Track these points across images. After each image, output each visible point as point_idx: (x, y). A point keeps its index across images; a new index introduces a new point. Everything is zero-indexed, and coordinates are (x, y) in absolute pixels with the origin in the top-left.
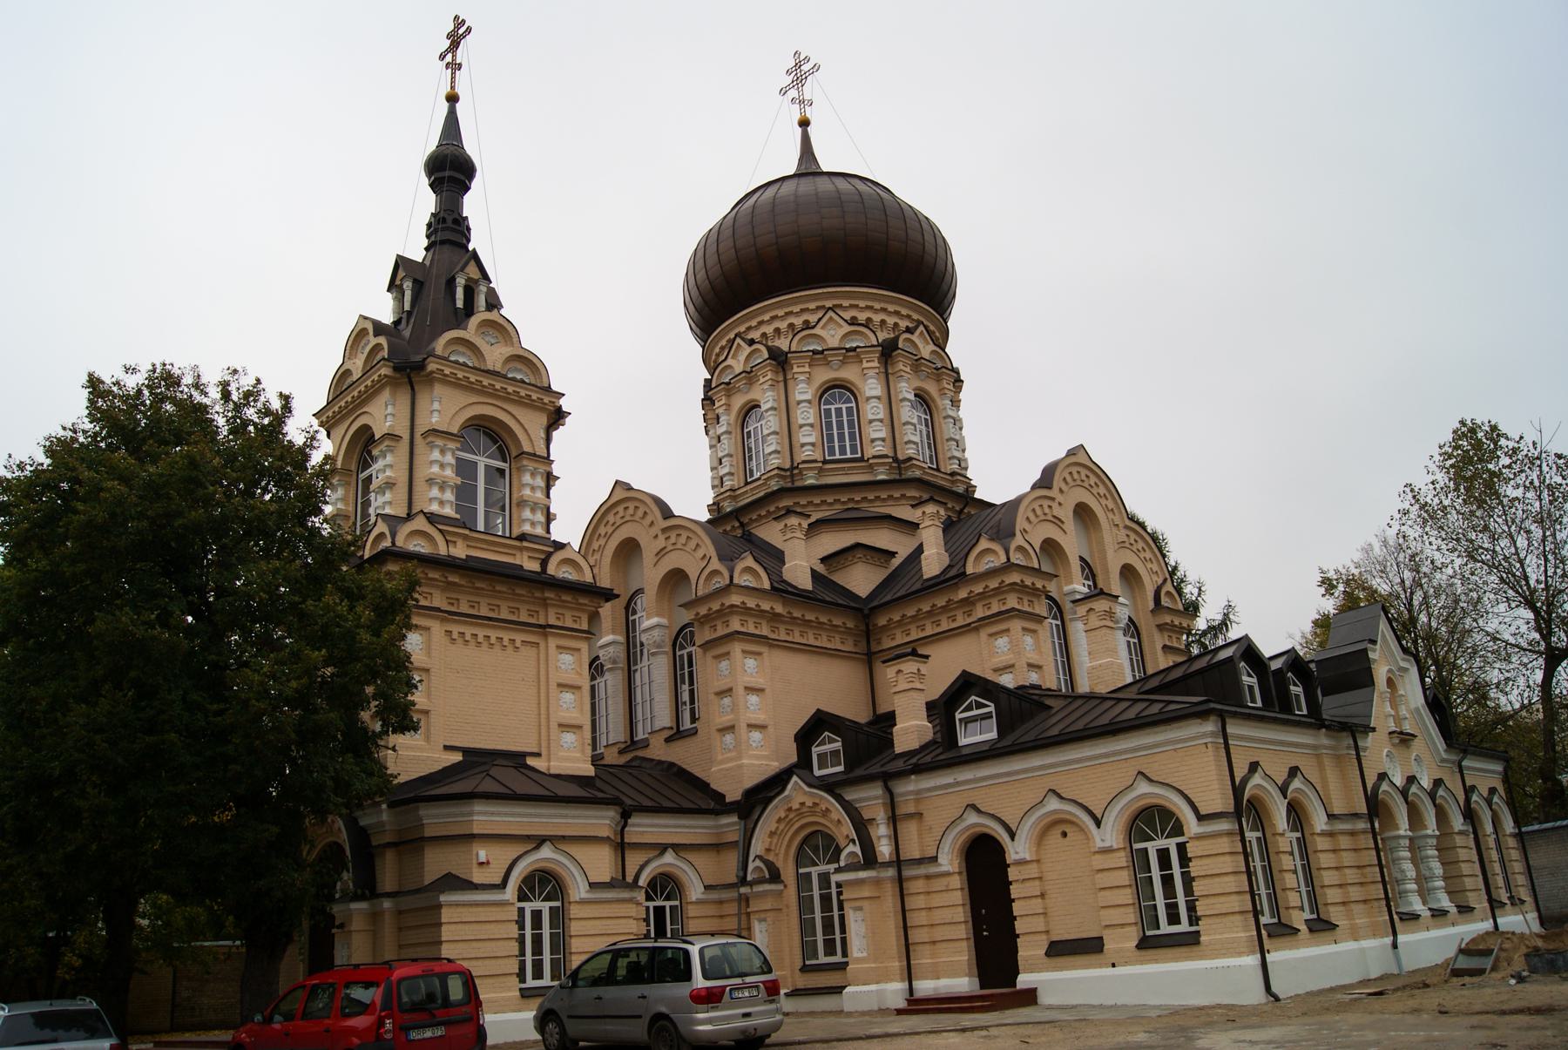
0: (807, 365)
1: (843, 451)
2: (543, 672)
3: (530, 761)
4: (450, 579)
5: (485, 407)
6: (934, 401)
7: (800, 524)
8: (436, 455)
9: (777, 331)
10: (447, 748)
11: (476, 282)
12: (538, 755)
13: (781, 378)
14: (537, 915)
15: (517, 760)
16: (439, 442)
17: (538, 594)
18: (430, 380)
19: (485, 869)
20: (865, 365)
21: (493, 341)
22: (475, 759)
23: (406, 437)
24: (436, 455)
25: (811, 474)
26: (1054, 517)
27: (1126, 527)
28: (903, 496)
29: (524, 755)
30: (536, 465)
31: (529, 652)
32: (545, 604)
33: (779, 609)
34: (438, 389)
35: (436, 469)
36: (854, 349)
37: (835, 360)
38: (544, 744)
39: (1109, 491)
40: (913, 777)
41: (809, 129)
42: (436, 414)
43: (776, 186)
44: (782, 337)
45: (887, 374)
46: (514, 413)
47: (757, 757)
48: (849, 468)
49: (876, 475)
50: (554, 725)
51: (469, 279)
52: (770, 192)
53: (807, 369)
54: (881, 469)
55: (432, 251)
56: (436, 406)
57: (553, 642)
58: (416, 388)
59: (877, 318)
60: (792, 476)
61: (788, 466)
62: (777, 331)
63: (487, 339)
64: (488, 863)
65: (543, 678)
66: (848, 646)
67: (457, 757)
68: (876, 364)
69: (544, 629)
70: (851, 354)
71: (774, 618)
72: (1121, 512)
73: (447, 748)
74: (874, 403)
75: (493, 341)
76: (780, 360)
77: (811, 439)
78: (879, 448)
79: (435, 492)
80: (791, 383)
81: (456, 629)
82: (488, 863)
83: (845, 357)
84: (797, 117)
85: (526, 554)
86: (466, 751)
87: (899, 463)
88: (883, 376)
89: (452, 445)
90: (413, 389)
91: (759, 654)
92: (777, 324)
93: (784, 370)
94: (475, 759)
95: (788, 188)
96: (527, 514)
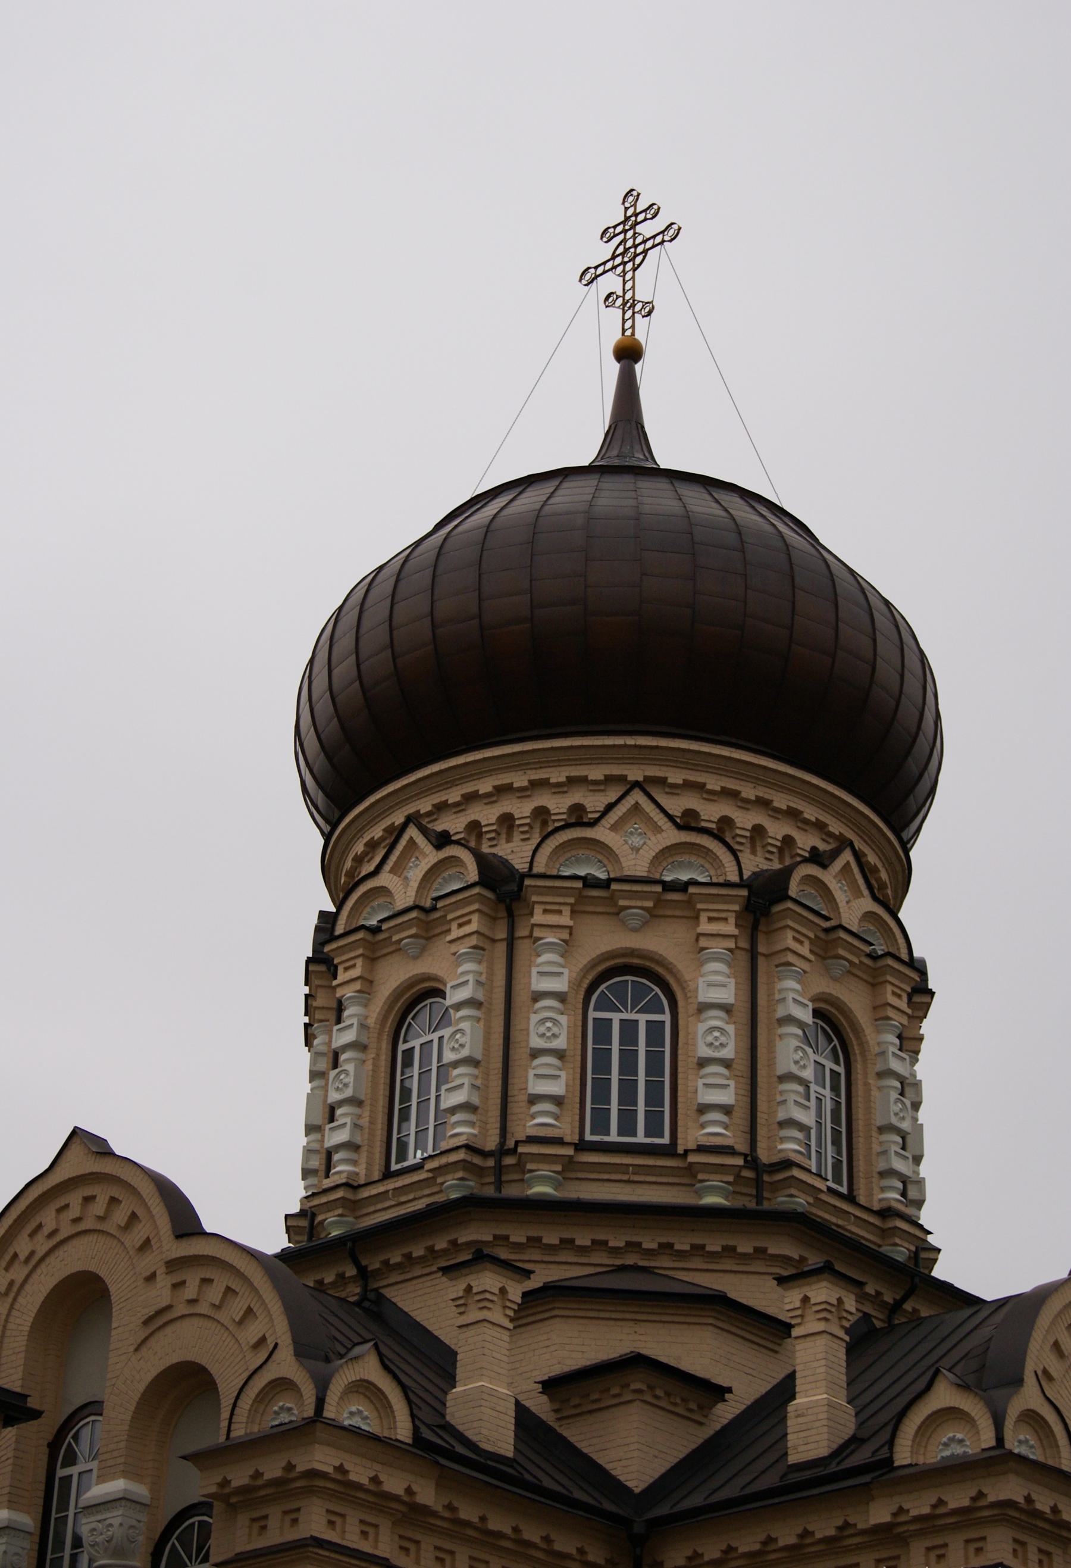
0: (566, 911)
1: (627, 1125)
9: (507, 821)
13: (502, 934)
20: (705, 927)
25: (545, 1170)
28: (760, 1252)
37: (636, 907)
41: (638, 367)
43: (549, 487)
44: (517, 837)
48: (639, 1169)
49: (699, 1194)
52: (531, 499)
54: (715, 1180)
60: (499, 1170)
68: (730, 928)
74: (715, 1019)
77: (556, 1088)
83: (659, 902)
84: (613, 336)
88: (743, 959)
92: (509, 805)
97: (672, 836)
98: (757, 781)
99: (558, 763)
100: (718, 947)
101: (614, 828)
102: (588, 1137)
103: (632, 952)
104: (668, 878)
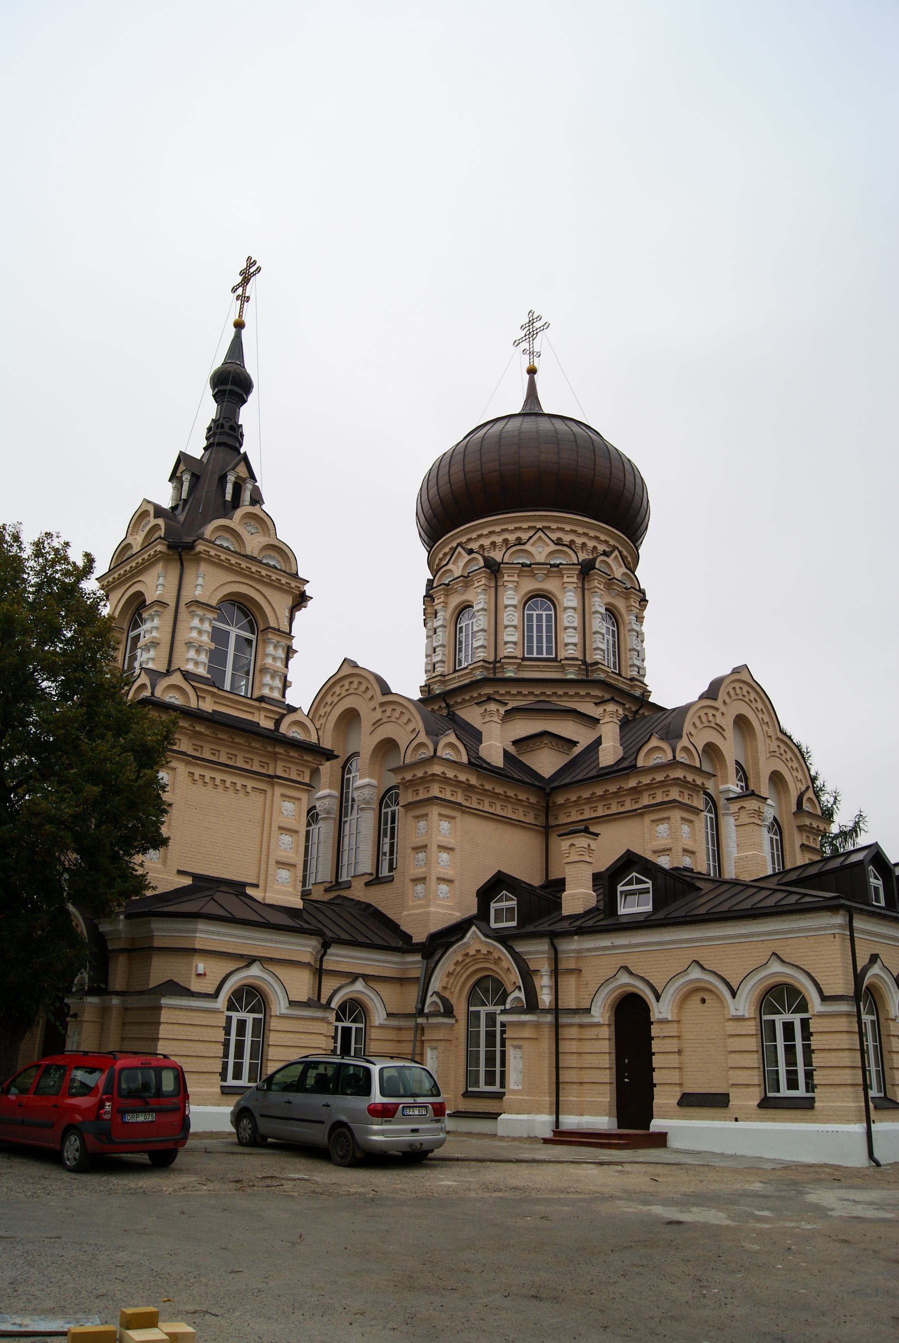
1: (540, 651)
2: (267, 816)
3: (249, 891)
4: (197, 729)
5: (245, 587)
6: (621, 615)
7: (498, 710)
8: (196, 622)
9: (493, 544)
10: (180, 872)
11: (244, 480)
12: (256, 886)
14: (242, 1024)
15: (238, 888)
16: (200, 612)
17: (270, 749)
18: (198, 559)
19: (201, 980)
21: (253, 531)
22: (203, 884)
23: (172, 605)
24: (196, 622)
25: (511, 668)
26: (717, 724)
27: (778, 739)
28: (588, 694)
29: (244, 885)
30: (279, 639)
31: (257, 798)
32: (275, 757)
33: (474, 781)
34: (204, 567)
35: (194, 634)
36: (557, 566)
37: (541, 573)
38: (262, 878)
39: (766, 706)
40: (576, 937)
42: (199, 588)
43: (505, 422)
44: (497, 550)
45: (496, 587)
46: (265, 593)
47: (443, 907)
50: (272, 862)
51: (238, 477)
52: (499, 426)
53: (515, 579)
54: (571, 670)
55: (209, 451)
56: (200, 581)
57: (278, 791)
58: (185, 565)
59: (579, 541)
60: (495, 668)
61: (491, 659)
62: (493, 544)
63: (248, 528)
64: (205, 974)
65: (267, 821)
66: (530, 819)
67: (188, 881)
68: (575, 580)
69: (272, 779)
70: (555, 569)
71: (468, 788)
72: (774, 726)
73: (180, 872)
74: (570, 612)
75: (253, 531)
76: (493, 569)
78: (571, 652)
79: (192, 654)
80: (500, 589)
81: (198, 772)
82: (205, 974)
83: (549, 571)
84: (526, 365)
85: (263, 714)
86: (196, 877)
87: (587, 666)
88: (579, 591)
89: (210, 616)
90: (182, 565)
91: (453, 818)
92: (494, 538)
93: (496, 578)
94: (203, 884)
95: (513, 424)
96: (267, 679)
97: (553, 547)
98: (583, 526)
99: (511, 523)
100: (571, 587)
101: (532, 545)
102: (526, 656)
103: (540, 590)
104: (552, 562)
